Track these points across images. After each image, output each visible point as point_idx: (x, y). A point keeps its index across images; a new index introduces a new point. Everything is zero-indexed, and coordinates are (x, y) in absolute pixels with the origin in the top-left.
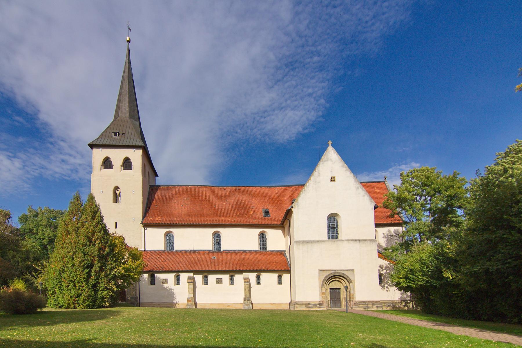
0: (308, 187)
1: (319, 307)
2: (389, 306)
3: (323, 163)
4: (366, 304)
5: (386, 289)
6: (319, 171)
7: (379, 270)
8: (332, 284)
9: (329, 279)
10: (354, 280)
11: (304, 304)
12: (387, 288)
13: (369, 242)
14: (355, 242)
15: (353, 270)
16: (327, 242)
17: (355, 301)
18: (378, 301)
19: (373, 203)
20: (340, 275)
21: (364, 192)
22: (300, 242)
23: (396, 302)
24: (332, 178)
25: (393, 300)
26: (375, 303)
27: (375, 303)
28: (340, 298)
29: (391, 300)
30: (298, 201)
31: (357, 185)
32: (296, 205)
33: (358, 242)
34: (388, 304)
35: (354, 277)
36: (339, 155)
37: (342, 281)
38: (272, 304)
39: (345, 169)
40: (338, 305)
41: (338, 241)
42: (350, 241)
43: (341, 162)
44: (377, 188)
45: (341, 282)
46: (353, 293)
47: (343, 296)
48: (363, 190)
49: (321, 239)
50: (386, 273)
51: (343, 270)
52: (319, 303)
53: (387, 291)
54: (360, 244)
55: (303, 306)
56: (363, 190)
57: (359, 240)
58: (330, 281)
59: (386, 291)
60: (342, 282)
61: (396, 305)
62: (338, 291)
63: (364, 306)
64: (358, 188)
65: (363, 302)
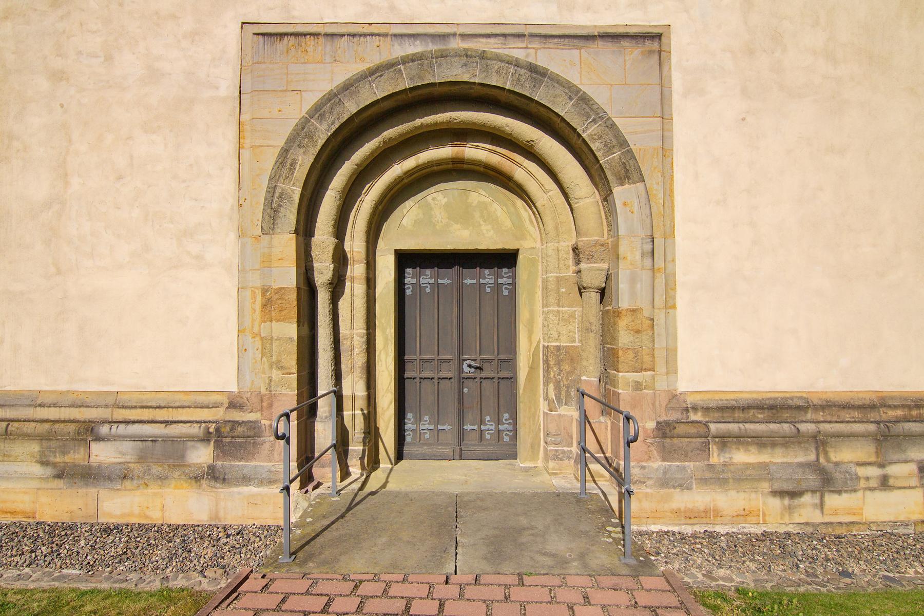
1: (214, 475)
4: (795, 440)
9: (392, 133)
10: (665, 151)
11: (26, 436)
17: (674, 397)
28: (511, 362)
35: (665, 117)
40: (489, 426)
45: (519, 191)
46: (643, 303)
47: (538, 334)
58: (396, 170)
60: (532, 187)
62: (499, 286)
63: (777, 457)
65: (759, 406)
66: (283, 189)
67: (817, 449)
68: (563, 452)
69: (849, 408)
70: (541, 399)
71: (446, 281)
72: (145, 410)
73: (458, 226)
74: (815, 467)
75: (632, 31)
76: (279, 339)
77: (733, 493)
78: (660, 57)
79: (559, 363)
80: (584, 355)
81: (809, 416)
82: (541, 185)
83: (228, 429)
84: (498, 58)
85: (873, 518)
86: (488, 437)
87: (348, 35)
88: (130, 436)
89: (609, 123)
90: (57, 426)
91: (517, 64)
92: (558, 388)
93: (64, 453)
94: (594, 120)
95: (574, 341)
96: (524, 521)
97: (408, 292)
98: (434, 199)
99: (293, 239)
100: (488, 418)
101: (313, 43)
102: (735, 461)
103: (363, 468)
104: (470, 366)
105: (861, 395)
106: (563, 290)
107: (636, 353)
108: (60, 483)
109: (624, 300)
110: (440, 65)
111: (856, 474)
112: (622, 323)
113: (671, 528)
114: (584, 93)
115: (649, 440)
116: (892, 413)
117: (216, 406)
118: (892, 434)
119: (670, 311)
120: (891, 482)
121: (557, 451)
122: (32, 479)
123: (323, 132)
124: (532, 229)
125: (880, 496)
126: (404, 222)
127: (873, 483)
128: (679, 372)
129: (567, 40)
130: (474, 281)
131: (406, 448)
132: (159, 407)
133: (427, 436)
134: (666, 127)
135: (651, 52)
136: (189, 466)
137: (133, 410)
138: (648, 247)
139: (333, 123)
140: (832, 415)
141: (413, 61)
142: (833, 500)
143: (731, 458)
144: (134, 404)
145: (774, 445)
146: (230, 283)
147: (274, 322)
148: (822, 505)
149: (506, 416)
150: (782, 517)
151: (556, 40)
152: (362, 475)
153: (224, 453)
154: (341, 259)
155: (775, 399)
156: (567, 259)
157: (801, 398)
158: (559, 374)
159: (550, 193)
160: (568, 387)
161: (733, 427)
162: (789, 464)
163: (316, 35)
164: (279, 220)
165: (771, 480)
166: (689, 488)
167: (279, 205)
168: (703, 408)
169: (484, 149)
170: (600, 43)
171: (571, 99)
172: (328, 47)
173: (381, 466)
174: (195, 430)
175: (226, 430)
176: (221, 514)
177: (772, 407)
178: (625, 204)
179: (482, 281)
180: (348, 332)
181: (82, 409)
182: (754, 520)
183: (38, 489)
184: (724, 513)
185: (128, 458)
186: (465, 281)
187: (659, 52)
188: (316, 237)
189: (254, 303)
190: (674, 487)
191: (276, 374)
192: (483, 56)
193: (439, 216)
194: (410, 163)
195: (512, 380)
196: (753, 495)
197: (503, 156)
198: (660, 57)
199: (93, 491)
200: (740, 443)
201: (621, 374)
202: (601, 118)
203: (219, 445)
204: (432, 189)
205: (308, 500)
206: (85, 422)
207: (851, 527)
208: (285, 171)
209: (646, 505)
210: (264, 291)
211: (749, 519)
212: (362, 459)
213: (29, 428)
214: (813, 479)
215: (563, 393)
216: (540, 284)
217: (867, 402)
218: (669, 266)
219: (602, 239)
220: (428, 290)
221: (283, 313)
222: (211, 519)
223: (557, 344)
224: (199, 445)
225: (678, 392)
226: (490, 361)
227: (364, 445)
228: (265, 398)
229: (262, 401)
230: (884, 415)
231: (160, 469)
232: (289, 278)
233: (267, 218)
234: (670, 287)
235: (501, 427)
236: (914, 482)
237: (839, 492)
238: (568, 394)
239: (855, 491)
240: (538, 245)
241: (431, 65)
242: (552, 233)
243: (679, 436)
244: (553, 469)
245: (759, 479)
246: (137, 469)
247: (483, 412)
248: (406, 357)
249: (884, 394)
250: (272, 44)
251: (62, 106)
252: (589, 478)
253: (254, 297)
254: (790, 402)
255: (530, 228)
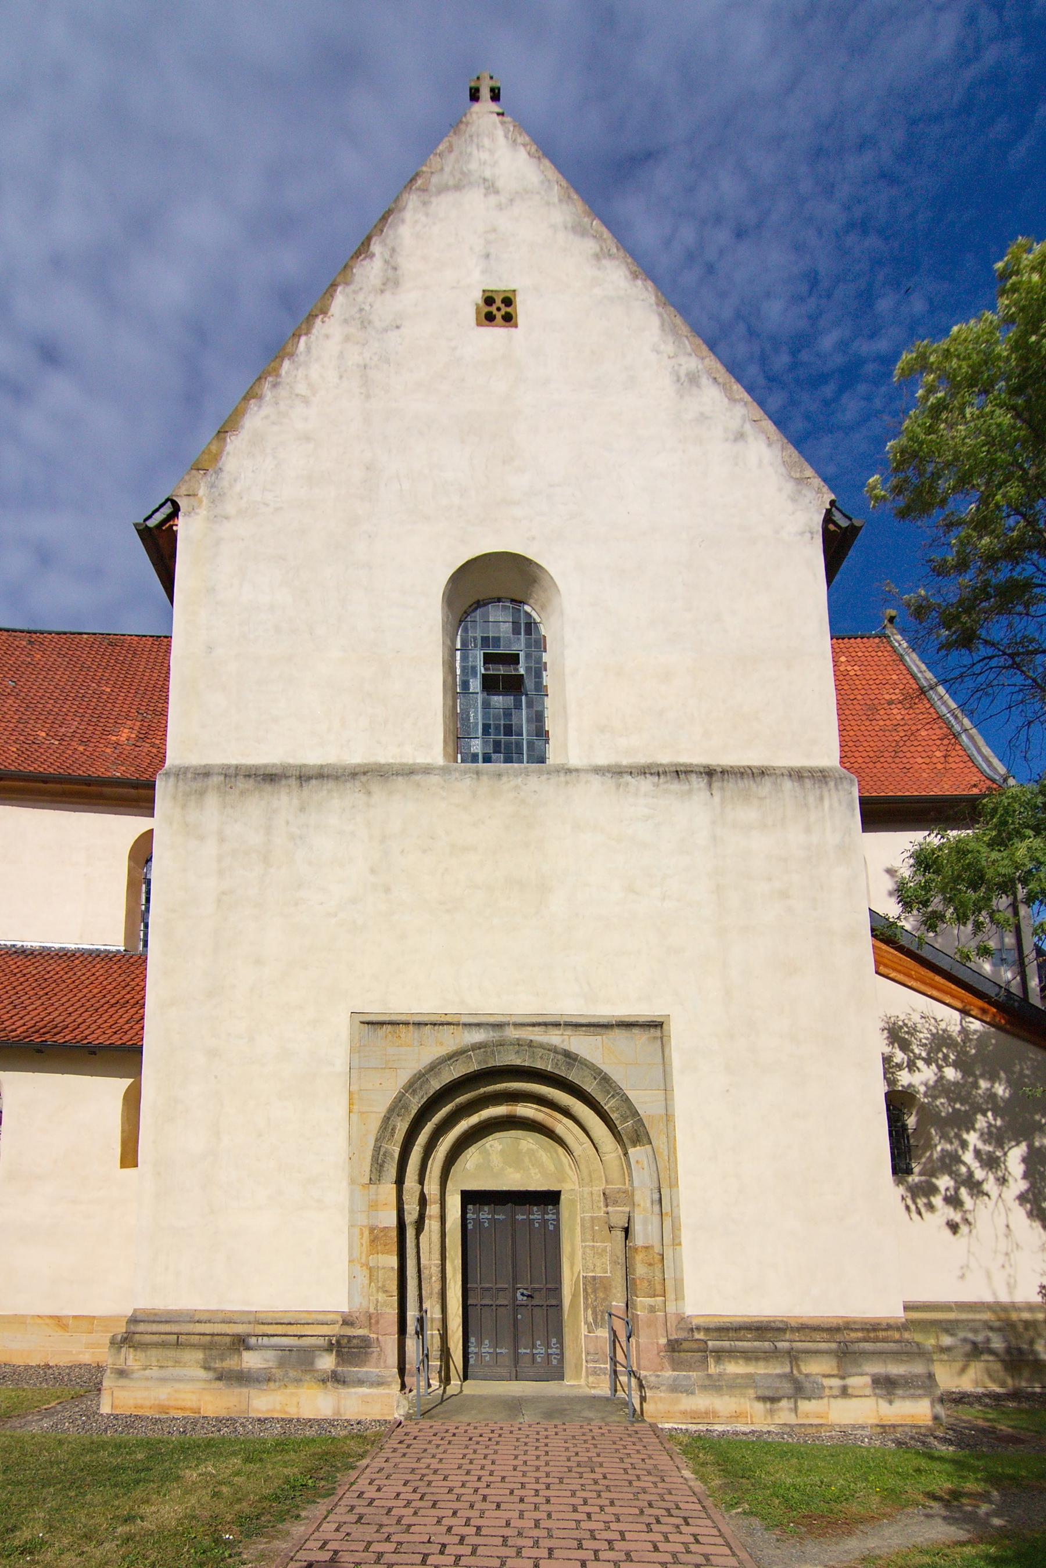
0: (302, 358)
1: (336, 1379)
2: (976, 1351)
3: (425, 203)
5: (946, 1212)
6: (393, 250)
7: (887, 1060)
8: (486, 1154)
10: (669, 1117)
11: (193, 1346)
12: (954, 1201)
13: (788, 785)
14: (675, 786)
15: (656, 1025)
16: (434, 779)
17: (682, 1319)
18: (889, 1327)
19: (810, 495)
20: (539, 1065)
21: (740, 410)
22: (205, 773)
23: (1026, 1316)
24: (489, 301)
25: (1004, 1298)
26: (868, 1346)
27: (868, 1346)
28: (556, 1291)
29: (989, 1298)
30: (220, 465)
31: (683, 360)
32: (201, 492)
33: (698, 783)
34: (970, 1336)
35: (667, 1089)
36: (547, 163)
37: (562, 1126)
38: (59, 1321)
39: (590, 246)
40: (540, 1350)
41: (540, 773)
42: (628, 778)
43: (560, 201)
44: (850, 659)
47: (579, 1266)
48: (725, 389)
49: (386, 756)
50: (940, 1087)
51: (568, 1025)
52: (335, 1330)
53: (954, 1227)
54: (717, 798)
55: (177, 1362)
56: (732, 400)
57: (710, 773)
58: (464, 1125)
59: (948, 1232)
60: (570, 1140)
61: (1031, 1342)
63: (760, 1369)
64: (693, 379)
66: (386, 1149)
67: (791, 1362)
68: (600, 1368)
69: (819, 1330)
70: (583, 1323)
71: (501, 1217)
72: (279, 1326)
73: (511, 1170)
74: (790, 1377)
75: (641, 1020)
76: (384, 1268)
77: (727, 1398)
78: (662, 1042)
79: (595, 1291)
80: (614, 1284)
81: (788, 1336)
82: (577, 1139)
83: (346, 1341)
84: (541, 1046)
85: (837, 1422)
86: (539, 1360)
87: (431, 1024)
88: (273, 1347)
89: (624, 1097)
90: (216, 1338)
91: (554, 1050)
92: (594, 1313)
93: (222, 1360)
94: (613, 1096)
95: (607, 1272)
96: (568, 1407)
97: (470, 1226)
98: (491, 1146)
99: (392, 1188)
100: (539, 1343)
101: (404, 1031)
102: (728, 1372)
103: (441, 1381)
104: (522, 1294)
105: (830, 1320)
106: (597, 1228)
107: (649, 1282)
108: (220, 1384)
109: (639, 1237)
110: (499, 1052)
111: (822, 1385)
112: (639, 1257)
113: (680, 1426)
114: (606, 1074)
115: (662, 1354)
116: (854, 1335)
117: (333, 1323)
118: (850, 1351)
119: (677, 1247)
120: (850, 1391)
121: (595, 1368)
122: (198, 1380)
123: (415, 1104)
124: (571, 1173)
125: (841, 1403)
126: (468, 1166)
127: (836, 1392)
128: (686, 1299)
129: (592, 1029)
130: (525, 1217)
131: (470, 1369)
132: (290, 1324)
133: (488, 1358)
134: (668, 1097)
135: (655, 1038)
136: (317, 1371)
137: (270, 1326)
138: (656, 1196)
139: (422, 1097)
140: (806, 1336)
141: (480, 1048)
142: (804, 1406)
143: (725, 1369)
144: (271, 1321)
145: (757, 1359)
146: (342, 1221)
147: (380, 1255)
148: (796, 1409)
149: (554, 1340)
150: (766, 1418)
151: (584, 1029)
152: (440, 1386)
153: (343, 1360)
154: (423, 1201)
155: (762, 1322)
156: (599, 1201)
157: (782, 1321)
158: (596, 1300)
159: (584, 1146)
160: (602, 1312)
161: (726, 1344)
162: (770, 1375)
163: (407, 1024)
164: (383, 1173)
165: (756, 1387)
166: (693, 1393)
167: (384, 1162)
168: (704, 1328)
169: (531, 1108)
170: (617, 1031)
171: (595, 1078)
172: (416, 1035)
173: (452, 1382)
174: (321, 1341)
175: (344, 1341)
176: (342, 1411)
177: (758, 1329)
178: (637, 1162)
179: (531, 1217)
180: (427, 1262)
181: (231, 1325)
182: (744, 1420)
183: (204, 1389)
184: (721, 1414)
185: (271, 1364)
186: (517, 1217)
187: (662, 1038)
188: (406, 1183)
189: (362, 1238)
190: (682, 1392)
191: (381, 1297)
192: (531, 1044)
193: (496, 1160)
194: (474, 1119)
195: (559, 1306)
196: (742, 1400)
197: (547, 1114)
198: (662, 1042)
199: (245, 1390)
200: (730, 1357)
201: (639, 1299)
202: (618, 1094)
203: (339, 1354)
204: (490, 1138)
205: (407, 1399)
206: (233, 1335)
207: (819, 1428)
208: (388, 1134)
209: (661, 1407)
210: (372, 1229)
211: (740, 1419)
212: (440, 1372)
213: (195, 1339)
214: (787, 1387)
215: (599, 1317)
216: (579, 1221)
217: (834, 1325)
218: (675, 1210)
219: (624, 1187)
220: (486, 1225)
221: (387, 1247)
222: (334, 1414)
223: (593, 1274)
224: (324, 1354)
225: (686, 1315)
226: (540, 1290)
227: (441, 1361)
228: (373, 1317)
229: (370, 1318)
230: (847, 1337)
231: (295, 1373)
232: (390, 1220)
233: (374, 1170)
234: (676, 1228)
235: (550, 1351)
236: (868, 1391)
237: (809, 1399)
238: (603, 1319)
239: (822, 1398)
240: (577, 1187)
241: (493, 1052)
242: (587, 1179)
243: (684, 1351)
244: (593, 1383)
245: (747, 1387)
246: (278, 1373)
247: (535, 1336)
248: (469, 1286)
249: (849, 1319)
250: (375, 1030)
251: (216, 1077)
252: (619, 1388)
253: (362, 1234)
254: (773, 1324)
255: (570, 1173)
